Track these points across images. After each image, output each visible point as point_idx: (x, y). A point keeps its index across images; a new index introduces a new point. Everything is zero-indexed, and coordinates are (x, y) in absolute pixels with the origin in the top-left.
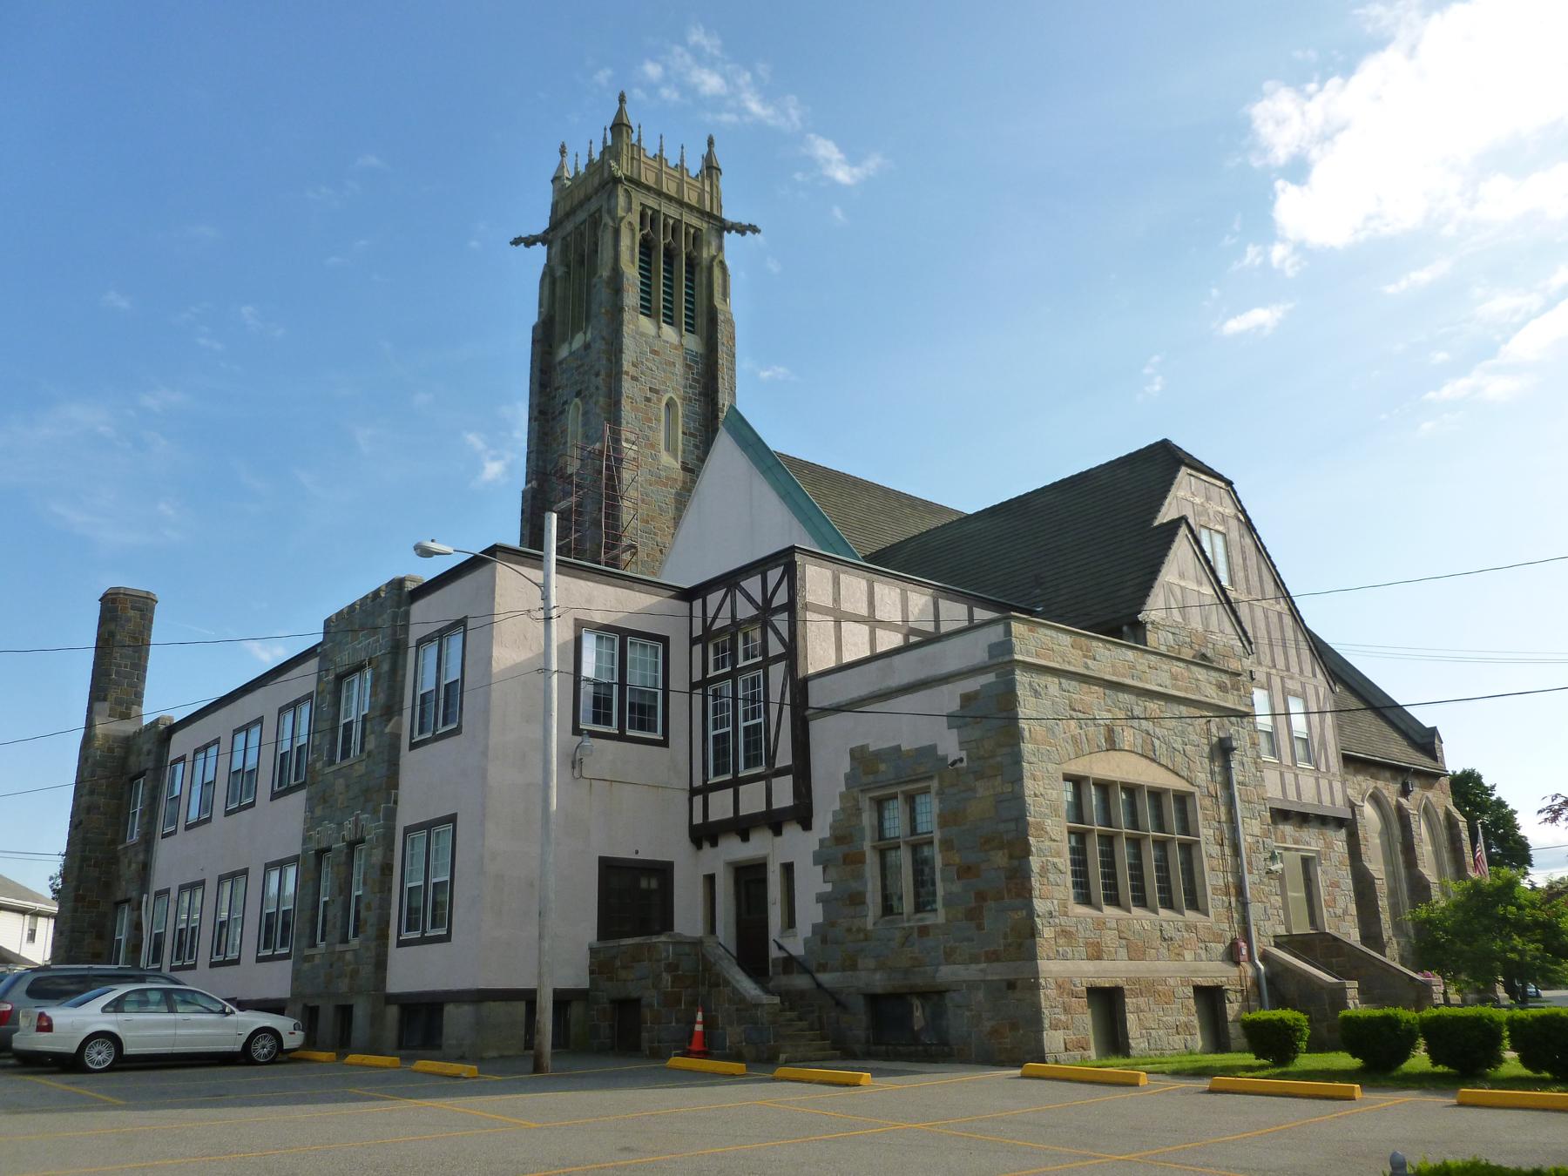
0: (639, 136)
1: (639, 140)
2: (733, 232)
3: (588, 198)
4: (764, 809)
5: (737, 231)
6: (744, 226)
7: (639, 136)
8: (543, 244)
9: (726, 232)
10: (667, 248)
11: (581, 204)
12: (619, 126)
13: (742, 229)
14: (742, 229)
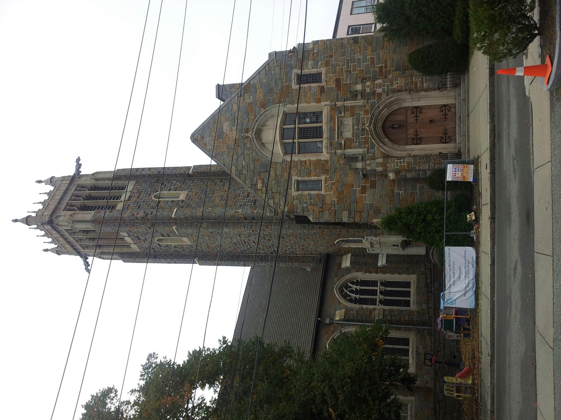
0: (32, 212)
1: (34, 212)
2: (80, 170)
3: (62, 236)
4: (331, 37)
5: (80, 167)
6: (77, 165)
7: (32, 212)
8: (88, 258)
9: (81, 174)
10: (84, 199)
11: (66, 239)
12: (27, 221)
13: (79, 166)
14: (79, 166)
